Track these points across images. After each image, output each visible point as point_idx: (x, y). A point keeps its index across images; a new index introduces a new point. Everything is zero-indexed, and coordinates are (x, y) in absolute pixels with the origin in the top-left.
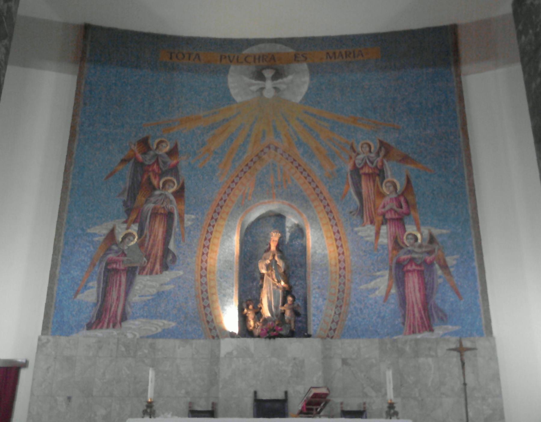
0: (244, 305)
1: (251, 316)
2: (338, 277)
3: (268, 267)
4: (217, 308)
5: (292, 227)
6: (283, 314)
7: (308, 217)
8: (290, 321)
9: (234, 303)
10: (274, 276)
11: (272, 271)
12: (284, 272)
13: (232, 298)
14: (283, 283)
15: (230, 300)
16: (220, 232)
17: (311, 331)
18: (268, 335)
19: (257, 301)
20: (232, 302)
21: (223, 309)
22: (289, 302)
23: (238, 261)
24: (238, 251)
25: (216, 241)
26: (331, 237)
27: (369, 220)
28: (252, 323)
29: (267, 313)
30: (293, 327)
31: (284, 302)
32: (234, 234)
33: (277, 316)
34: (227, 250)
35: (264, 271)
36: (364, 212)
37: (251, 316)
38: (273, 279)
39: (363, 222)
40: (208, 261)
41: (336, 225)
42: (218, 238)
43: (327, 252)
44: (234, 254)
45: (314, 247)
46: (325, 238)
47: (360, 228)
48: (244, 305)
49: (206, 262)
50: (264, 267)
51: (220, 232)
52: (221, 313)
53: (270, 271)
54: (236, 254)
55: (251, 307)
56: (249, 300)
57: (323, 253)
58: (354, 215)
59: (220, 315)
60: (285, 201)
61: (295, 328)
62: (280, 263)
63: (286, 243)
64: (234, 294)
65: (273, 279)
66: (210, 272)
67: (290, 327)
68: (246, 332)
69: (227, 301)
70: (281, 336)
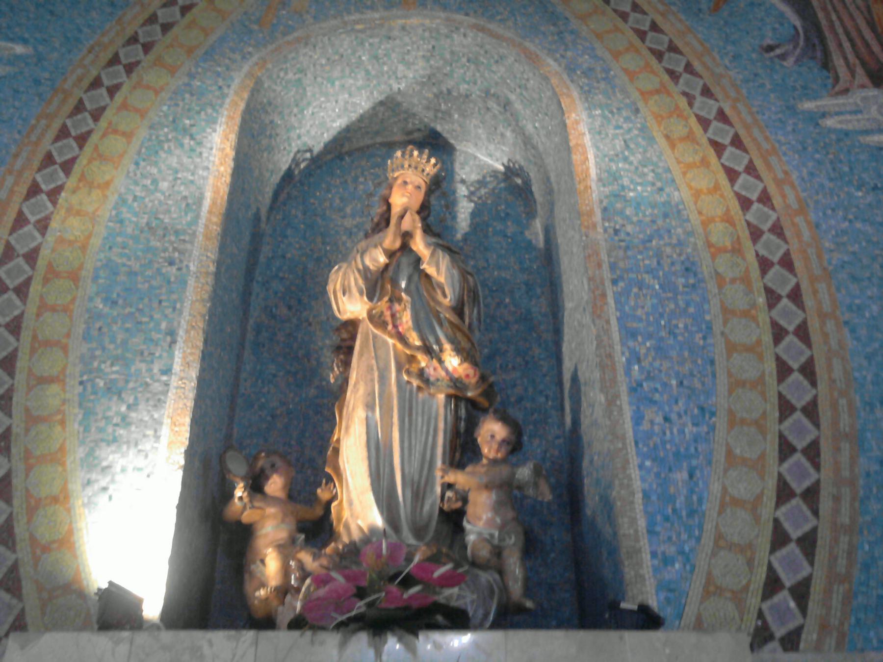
0: (237, 466)
1: (271, 529)
2: (761, 300)
3: (376, 285)
4: (57, 457)
5: (482, 183)
6: (453, 520)
7: (571, 69)
8: (498, 552)
9: (165, 431)
10: (406, 319)
11: (395, 299)
12: (458, 310)
13: (159, 404)
14: (453, 361)
15: (142, 414)
16: (142, 113)
17: (644, 588)
18: (360, 607)
19: (313, 469)
20: (157, 424)
21: (91, 462)
22: (488, 450)
23: (216, 229)
24: (224, 190)
25: (114, 144)
26: (690, 137)
27: (859, 71)
28: (271, 566)
29: (359, 509)
30: (516, 589)
31: (463, 449)
32: (212, 122)
33: (419, 532)
34: (164, 185)
35: (352, 306)
36: (832, 46)
37: (271, 529)
38: (402, 338)
39: (837, 79)
40: (54, 224)
41: (706, 92)
42: (128, 136)
43: (681, 194)
44: (199, 201)
45: (610, 177)
46: (662, 142)
47: (827, 102)
48: (237, 466)
49: (43, 226)
50: (355, 281)
51: (142, 113)
52: (75, 486)
53: (383, 304)
54: (208, 195)
55: (275, 485)
56: (263, 423)
57: (661, 198)
58: (783, 57)
59: (62, 498)
60: (460, 17)
61: (528, 590)
62: (439, 269)
63: (459, 236)
64: (174, 382)
65: (402, 338)
66: (52, 273)
67: (505, 589)
68: (215, 580)
69: (125, 421)
70: (458, 620)
